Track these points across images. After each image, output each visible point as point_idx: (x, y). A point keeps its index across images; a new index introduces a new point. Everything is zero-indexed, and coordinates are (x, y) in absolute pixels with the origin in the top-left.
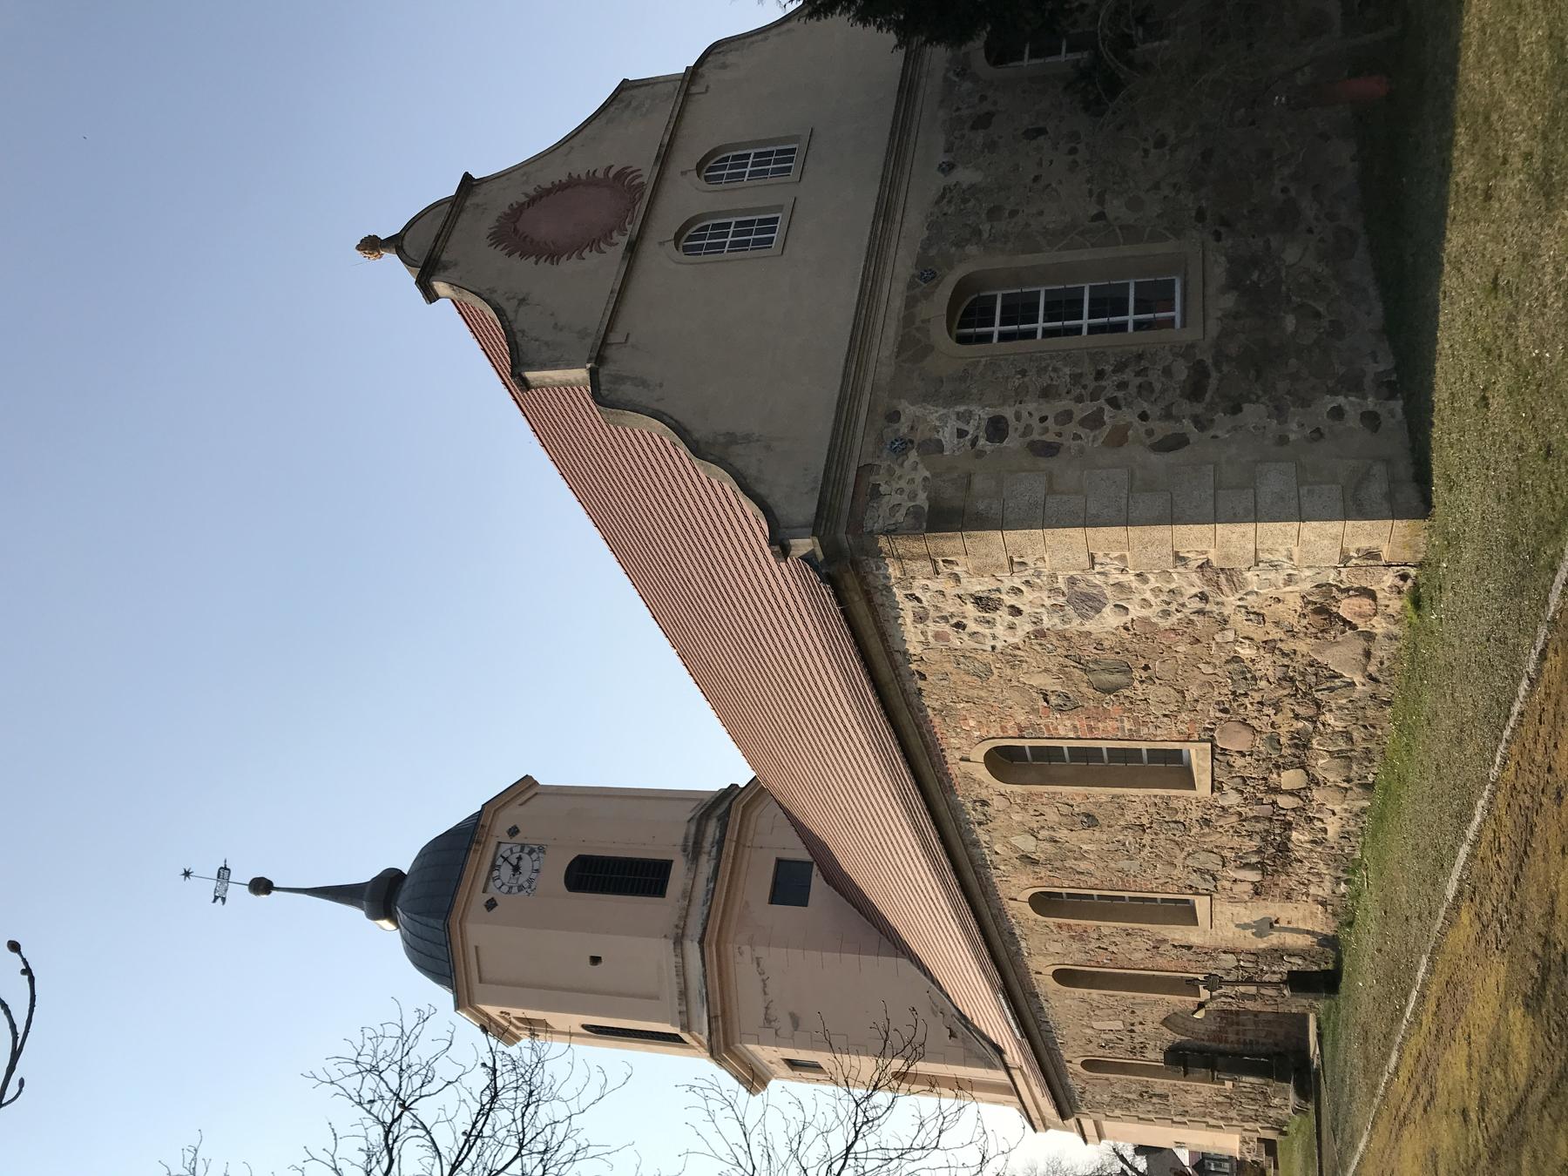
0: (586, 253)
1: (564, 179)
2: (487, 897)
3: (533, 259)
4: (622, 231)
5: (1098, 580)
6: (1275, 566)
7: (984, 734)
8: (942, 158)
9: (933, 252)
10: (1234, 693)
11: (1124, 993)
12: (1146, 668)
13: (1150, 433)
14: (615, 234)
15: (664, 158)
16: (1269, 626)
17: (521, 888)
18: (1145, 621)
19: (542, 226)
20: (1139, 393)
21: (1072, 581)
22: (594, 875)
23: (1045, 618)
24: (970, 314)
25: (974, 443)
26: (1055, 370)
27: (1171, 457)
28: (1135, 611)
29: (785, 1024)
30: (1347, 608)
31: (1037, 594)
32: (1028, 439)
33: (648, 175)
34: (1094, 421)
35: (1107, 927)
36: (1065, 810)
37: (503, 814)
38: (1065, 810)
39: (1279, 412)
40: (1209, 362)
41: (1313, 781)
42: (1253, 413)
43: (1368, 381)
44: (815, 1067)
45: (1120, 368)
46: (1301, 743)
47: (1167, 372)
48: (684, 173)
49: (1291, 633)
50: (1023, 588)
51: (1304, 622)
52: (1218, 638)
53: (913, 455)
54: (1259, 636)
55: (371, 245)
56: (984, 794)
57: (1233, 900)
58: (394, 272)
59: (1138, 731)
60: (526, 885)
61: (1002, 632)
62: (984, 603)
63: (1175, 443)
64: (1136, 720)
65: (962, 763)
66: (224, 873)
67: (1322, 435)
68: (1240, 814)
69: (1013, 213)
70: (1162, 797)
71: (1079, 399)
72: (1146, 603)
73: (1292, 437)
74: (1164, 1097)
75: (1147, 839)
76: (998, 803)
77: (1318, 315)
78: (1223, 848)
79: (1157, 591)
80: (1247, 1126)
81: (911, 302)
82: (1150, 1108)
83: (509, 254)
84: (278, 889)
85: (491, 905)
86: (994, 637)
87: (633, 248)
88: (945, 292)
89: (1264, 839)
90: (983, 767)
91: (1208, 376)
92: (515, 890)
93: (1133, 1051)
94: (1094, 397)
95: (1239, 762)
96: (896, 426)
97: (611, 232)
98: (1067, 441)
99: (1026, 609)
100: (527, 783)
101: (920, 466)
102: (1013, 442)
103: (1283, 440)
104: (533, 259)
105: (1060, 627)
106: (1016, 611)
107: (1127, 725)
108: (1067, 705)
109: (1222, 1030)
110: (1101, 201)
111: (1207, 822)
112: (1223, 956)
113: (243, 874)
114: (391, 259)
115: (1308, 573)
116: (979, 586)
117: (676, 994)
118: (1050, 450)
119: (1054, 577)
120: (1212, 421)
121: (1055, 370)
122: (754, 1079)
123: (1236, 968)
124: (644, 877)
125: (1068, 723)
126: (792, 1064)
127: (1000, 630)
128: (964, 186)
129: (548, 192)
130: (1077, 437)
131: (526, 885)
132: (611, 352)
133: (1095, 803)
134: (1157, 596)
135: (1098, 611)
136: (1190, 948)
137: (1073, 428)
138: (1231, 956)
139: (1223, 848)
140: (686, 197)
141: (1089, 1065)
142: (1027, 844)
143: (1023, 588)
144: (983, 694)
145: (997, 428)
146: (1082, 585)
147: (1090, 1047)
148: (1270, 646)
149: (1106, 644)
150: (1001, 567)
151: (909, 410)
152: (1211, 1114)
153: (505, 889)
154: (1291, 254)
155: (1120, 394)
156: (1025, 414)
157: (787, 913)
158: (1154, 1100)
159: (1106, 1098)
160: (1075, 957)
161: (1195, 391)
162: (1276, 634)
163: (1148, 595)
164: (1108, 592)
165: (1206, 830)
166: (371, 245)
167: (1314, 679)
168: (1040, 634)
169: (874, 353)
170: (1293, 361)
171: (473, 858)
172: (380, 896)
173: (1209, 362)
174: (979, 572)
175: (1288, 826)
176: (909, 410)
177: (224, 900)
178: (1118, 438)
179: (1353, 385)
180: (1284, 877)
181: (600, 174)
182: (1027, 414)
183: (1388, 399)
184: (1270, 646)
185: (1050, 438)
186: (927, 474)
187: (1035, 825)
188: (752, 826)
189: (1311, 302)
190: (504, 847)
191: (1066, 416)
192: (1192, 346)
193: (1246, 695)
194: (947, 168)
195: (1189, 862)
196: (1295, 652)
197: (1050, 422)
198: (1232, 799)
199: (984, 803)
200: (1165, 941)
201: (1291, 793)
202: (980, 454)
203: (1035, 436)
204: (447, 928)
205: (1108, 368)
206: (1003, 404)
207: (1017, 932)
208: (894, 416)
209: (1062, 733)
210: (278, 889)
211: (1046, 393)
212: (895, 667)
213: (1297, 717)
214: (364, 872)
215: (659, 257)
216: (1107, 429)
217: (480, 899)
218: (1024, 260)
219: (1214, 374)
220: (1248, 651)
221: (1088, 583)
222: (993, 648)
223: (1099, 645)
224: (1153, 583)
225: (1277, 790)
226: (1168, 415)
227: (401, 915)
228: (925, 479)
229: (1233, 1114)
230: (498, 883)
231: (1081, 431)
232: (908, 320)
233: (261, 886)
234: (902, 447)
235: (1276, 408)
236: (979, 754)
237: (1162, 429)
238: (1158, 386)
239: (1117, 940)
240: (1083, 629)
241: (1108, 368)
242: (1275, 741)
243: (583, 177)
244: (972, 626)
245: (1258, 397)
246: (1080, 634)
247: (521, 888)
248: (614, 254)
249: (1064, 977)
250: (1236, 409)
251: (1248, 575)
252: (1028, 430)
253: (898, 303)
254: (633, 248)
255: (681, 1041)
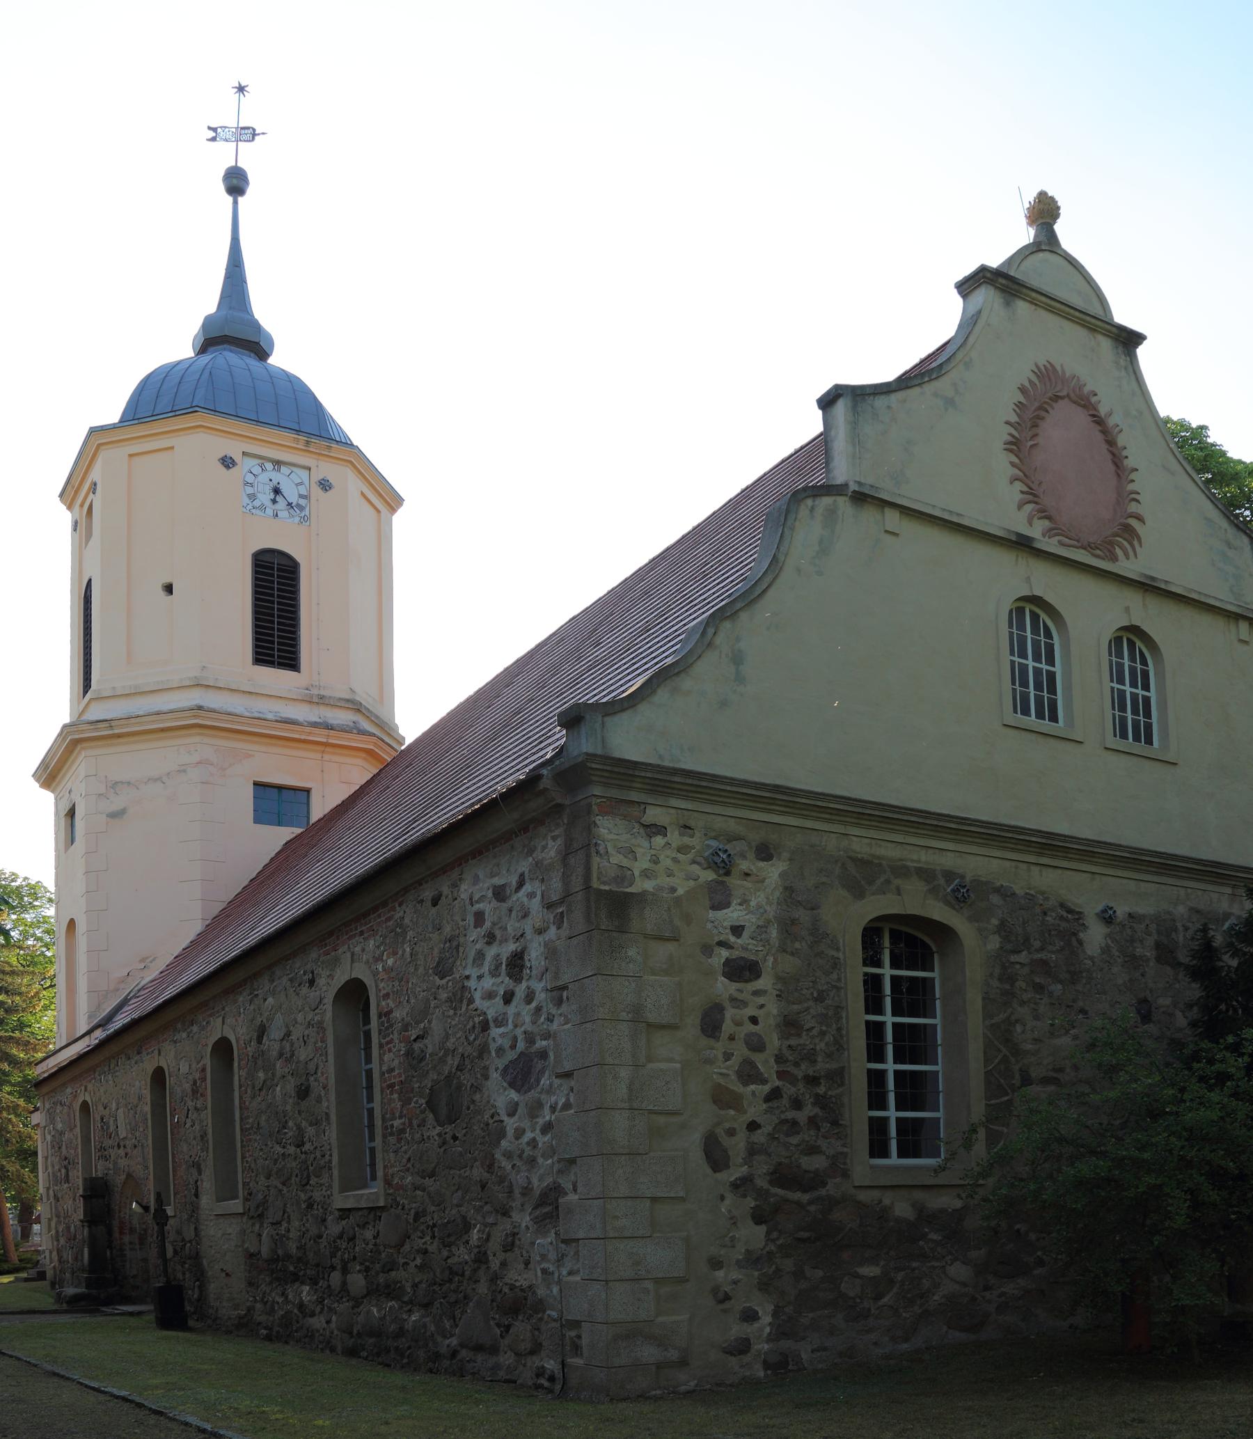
0: (1019, 486)
1: (1130, 463)
2: (237, 457)
3: (1014, 418)
4: (1048, 533)
5: (545, 1081)
6: (560, 1260)
7: (380, 976)
8: (1121, 911)
9: (995, 899)
10: (434, 1225)
11: (150, 1138)
12: (455, 1138)
13: (731, 1132)
14: (1047, 523)
15: (1148, 587)
16: (501, 1256)
17: (252, 497)
18: (502, 1134)
19: (1063, 431)
20: (785, 1121)
21: (543, 1055)
22: (276, 583)
23: (502, 1030)
24: (911, 941)
25: (721, 944)
26: (823, 1033)
27: (697, 1156)
28: (511, 1124)
29: (117, 803)
30: (521, 1328)
31: (528, 1019)
32: (727, 1004)
33: (1127, 567)
34: (749, 1074)
35: (207, 1117)
36: (312, 1066)
37: (350, 474)
38: (312, 1066)
39: (752, 1260)
40: (823, 1192)
41: (357, 1303)
42: (753, 1235)
43: (786, 1344)
44: (72, 840)
45: (820, 1101)
46: (391, 1291)
47: (813, 1150)
48: (1127, 609)
49: (494, 1279)
50: (534, 1005)
51: (506, 1290)
52: (487, 1208)
53: (710, 876)
54: (494, 1246)
55: (1044, 212)
56: (321, 982)
57: (243, 1232)
58: (1004, 240)
59: (392, 1134)
60: (257, 503)
61: (484, 984)
62: (516, 964)
63: (715, 1156)
64: (402, 1131)
65: (349, 955)
66: (248, 134)
67: (721, 1302)
68: (320, 1237)
69: (1039, 988)
70: (330, 1161)
71: (779, 1059)
72: (519, 1133)
73: (720, 1274)
74: (67, 1180)
75: (292, 1150)
76: (313, 995)
77: (878, 1298)
78: (289, 1222)
79: (533, 1143)
80: (55, 1253)
81: (926, 874)
82: (57, 1168)
83: (1022, 390)
84: (235, 203)
85: (228, 462)
86: (480, 977)
87: (1022, 544)
88: (938, 911)
89: (299, 1259)
90: (347, 978)
91: (805, 1191)
92: (250, 490)
93: (102, 1149)
94: (781, 1075)
95: (369, 1234)
96: (751, 855)
97: (1049, 518)
98: (720, 1047)
99: (511, 1010)
100: (393, 501)
101: (692, 883)
102: (723, 987)
103: (716, 1264)
104: (1014, 418)
105: (493, 1047)
106: (508, 998)
107: (397, 1123)
108: (414, 1059)
109: (132, 1230)
110: (1046, 1081)
111: (310, 1206)
112: (192, 1227)
113: (249, 158)
114: (1025, 235)
115: (555, 1290)
116: (535, 955)
117: (202, 704)
118: (711, 1023)
119: (547, 1036)
120: (745, 1196)
121: (823, 1033)
122: (49, 774)
123: (183, 1240)
124: (276, 637)
125: (396, 1062)
126: (71, 813)
127: (488, 983)
128: (1081, 935)
129: (1111, 443)
130: (728, 1056)
131: (257, 503)
132: (869, 515)
133: (320, 1096)
134: (528, 1144)
135: (512, 1085)
136: (197, 1195)
137: (740, 1051)
138: (193, 1233)
139: (289, 1222)
140: (1091, 614)
141: (85, 1107)
142: (275, 1032)
143: (534, 1005)
144: (421, 970)
145: (743, 970)
146: (539, 1066)
147: (101, 1108)
148: (481, 1258)
149: (477, 1097)
150: (556, 976)
151: (773, 872)
152: (59, 1222)
153: (250, 478)
154: (959, 1271)
155: (785, 1101)
156: (761, 1000)
157: (246, 797)
158: (63, 1171)
159: (59, 1126)
160: (178, 1085)
161: (784, 1177)
162: (495, 1264)
163: (528, 1135)
164: (533, 1094)
165: (304, 1206)
166: (1044, 212)
167: (452, 1300)
168: (485, 1026)
169: (856, 831)
170: (820, 1273)
171: (287, 438)
172: (233, 334)
173: (823, 1192)
174: (551, 952)
175: (314, 1282)
176: (773, 872)
177: (213, 139)
178: (722, 1098)
179: (783, 1330)
180: (267, 1279)
181: (1133, 508)
182: (763, 1002)
183: (765, 1362)
184: (481, 1258)
185: (728, 1027)
186: (680, 891)
187: (293, 1037)
188: (348, 760)
189: (895, 1290)
190: (304, 474)
191: (1211, 1062)
192: (846, 1174)
193: (433, 1237)
194: (1107, 917)
195: (273, 1191)
196: (477, 1281)
197: (753, 1028)
198: (334, 1228)
199: (312, 982)
200: (200, 1173)
201: (344, 1283)
202: (707, 950)
203: (730, 1013)
204: (191, 410)
205: (821, 1090)
206: (779, 978)
207: (195, 1028)
208: (765, 853)
209: (386, 1058)
210: (235, 203)
211: (790, 1025)
212: (444, 870)
213: (415, 1286)
214: (266, 308)
215: (1013, 577)
216: (738, 1088)
217: (234, 449)
218: (974, 1000)
219: (805, 1197)
220: (475, 1237)
221: (542, 1072)
222: (468, 977)
223: (476, 1088)
224: (543, 1140)
225: (345, 1271)
226: (752, 1151)
227: (206, 358)
228: (673, 890)
229: (62, 1241)
230: (257, 470)
231: (735, 1062)
232: (901, 871)
233: (236, 183)
234: (723, 866)
235: (758, 1259)
236: (361, 972)
237: (737, 1145)
238: (794, 1140)
239: (197, 1127)
240: (492, 1070)
241: (821, 1090)
242: (390, 1267)
243: (1131, 487)
244: (491, 952)
245: (773, 1241)
246: (486, 1068)
247: (252, 497)
248: (1018, 521)
249: (159, 1077)
250: (758, 1218)
251: (551, 1237)
252: (737, 1002)
253: (925, 858)
254: (1022, 544)
255: (85, 692)
